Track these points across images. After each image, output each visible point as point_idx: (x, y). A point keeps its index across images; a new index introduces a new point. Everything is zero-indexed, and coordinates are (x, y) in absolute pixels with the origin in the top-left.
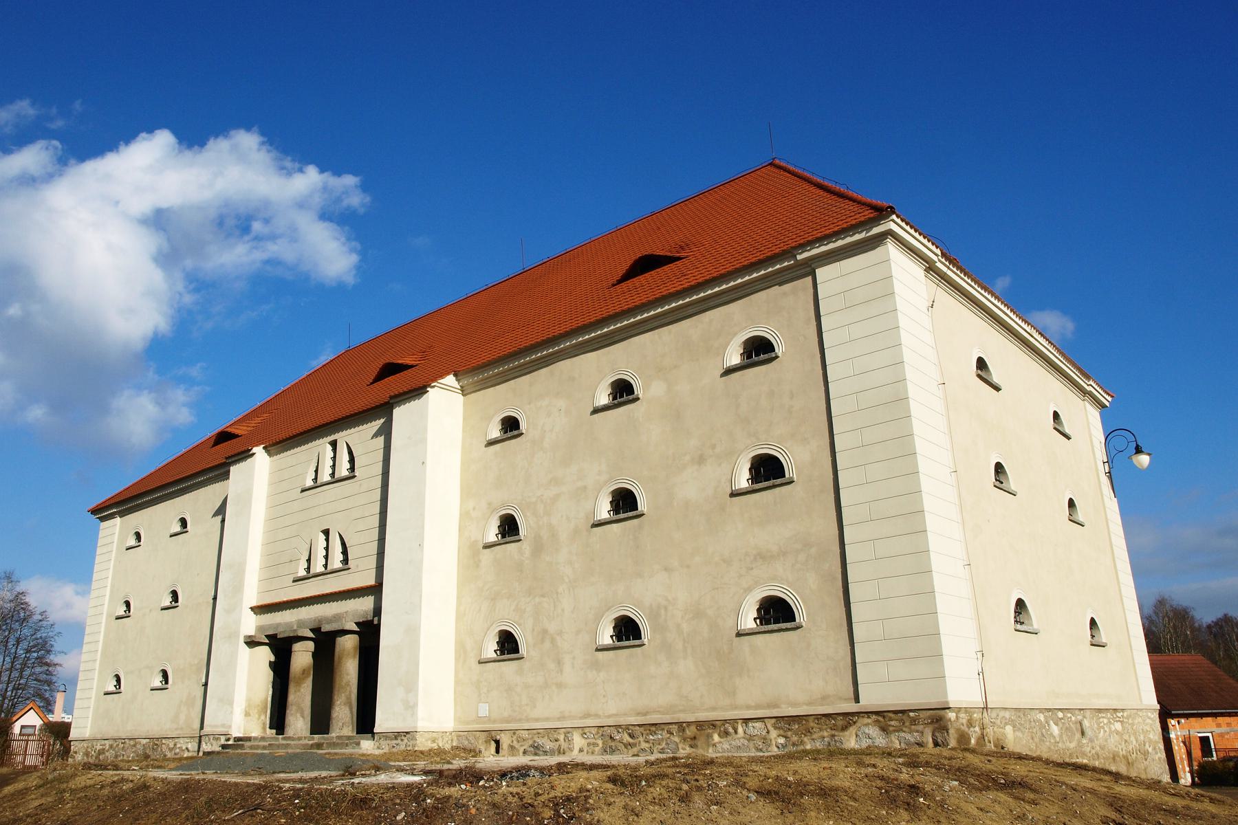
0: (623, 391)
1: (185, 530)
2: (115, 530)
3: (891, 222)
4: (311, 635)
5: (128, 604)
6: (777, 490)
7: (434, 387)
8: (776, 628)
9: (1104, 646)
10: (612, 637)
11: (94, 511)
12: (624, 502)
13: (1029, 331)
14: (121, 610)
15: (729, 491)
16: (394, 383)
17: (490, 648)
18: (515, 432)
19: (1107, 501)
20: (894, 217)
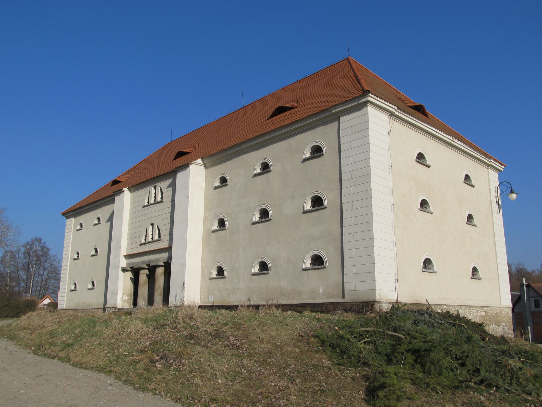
0: (265, 167)
1: (99, 223)
2: (72, 223)
3: (369, 97)
4: (147, 267)
5: (78, 254)
6: (320, 211)
7: (192, 164)
8: (316, 268)
9: (480, 279)
10: (258, 269)
11: (64, 214)
12: (264, 214)
13: (451, 139)
14: (76, 257)
15: (302, 211)
16: (181, 160)
17: (214, 273)
18: (225, 184)
19: (495, 215)
20: (370, 95)
